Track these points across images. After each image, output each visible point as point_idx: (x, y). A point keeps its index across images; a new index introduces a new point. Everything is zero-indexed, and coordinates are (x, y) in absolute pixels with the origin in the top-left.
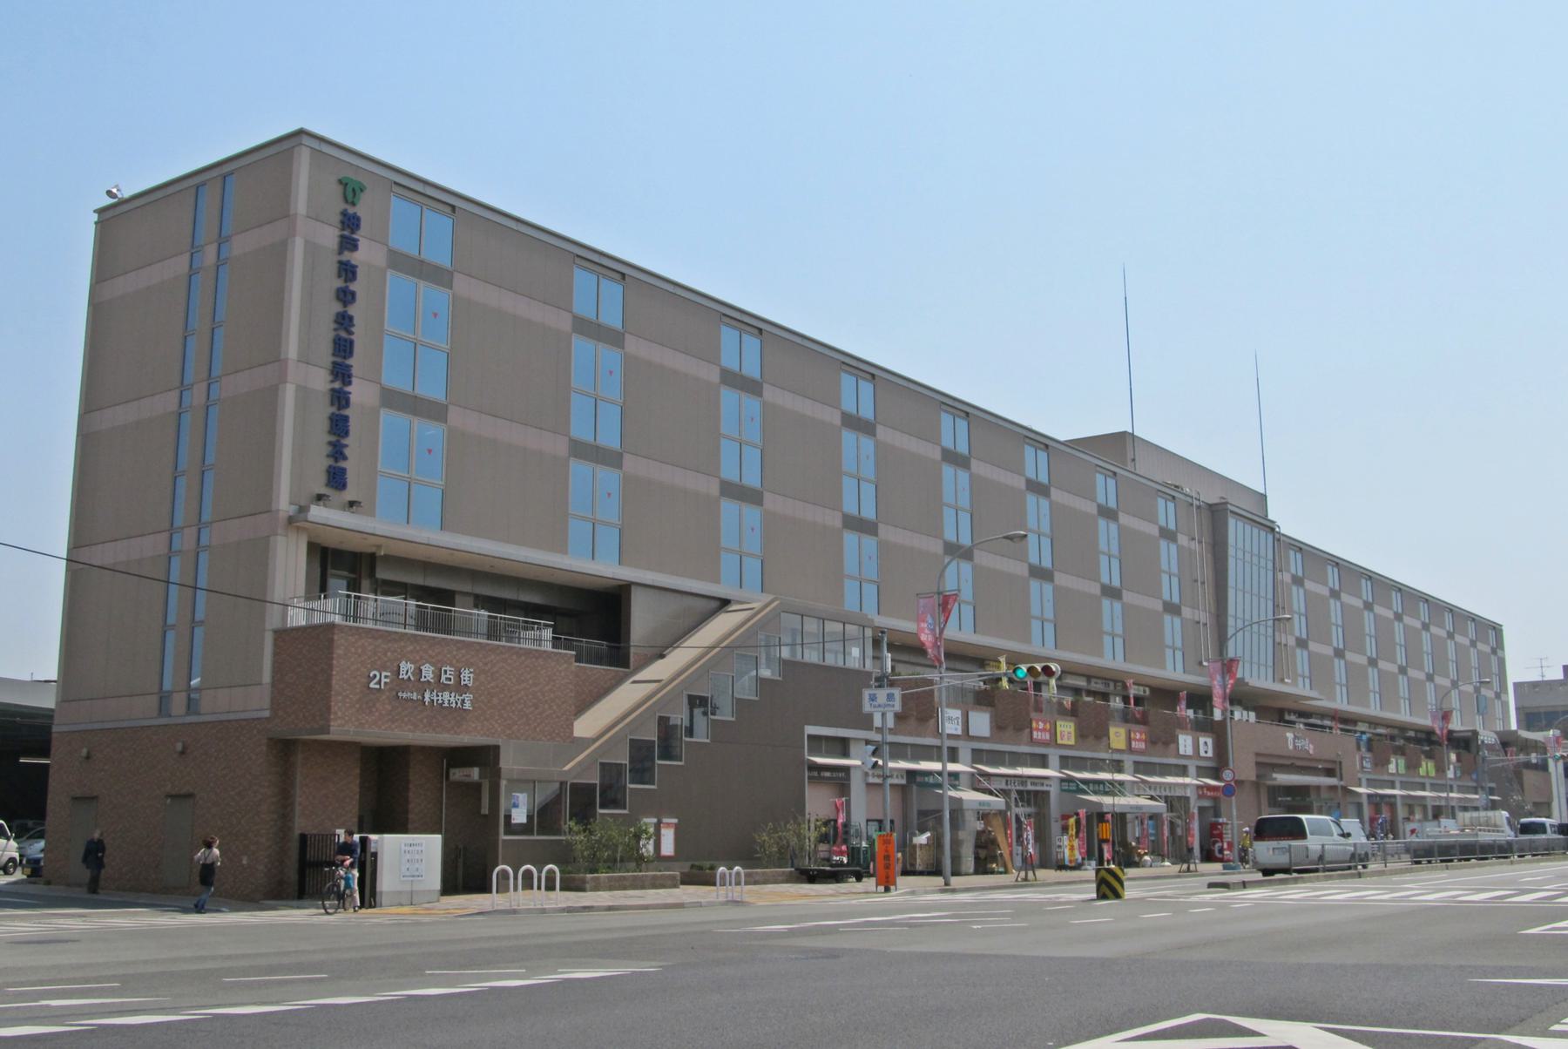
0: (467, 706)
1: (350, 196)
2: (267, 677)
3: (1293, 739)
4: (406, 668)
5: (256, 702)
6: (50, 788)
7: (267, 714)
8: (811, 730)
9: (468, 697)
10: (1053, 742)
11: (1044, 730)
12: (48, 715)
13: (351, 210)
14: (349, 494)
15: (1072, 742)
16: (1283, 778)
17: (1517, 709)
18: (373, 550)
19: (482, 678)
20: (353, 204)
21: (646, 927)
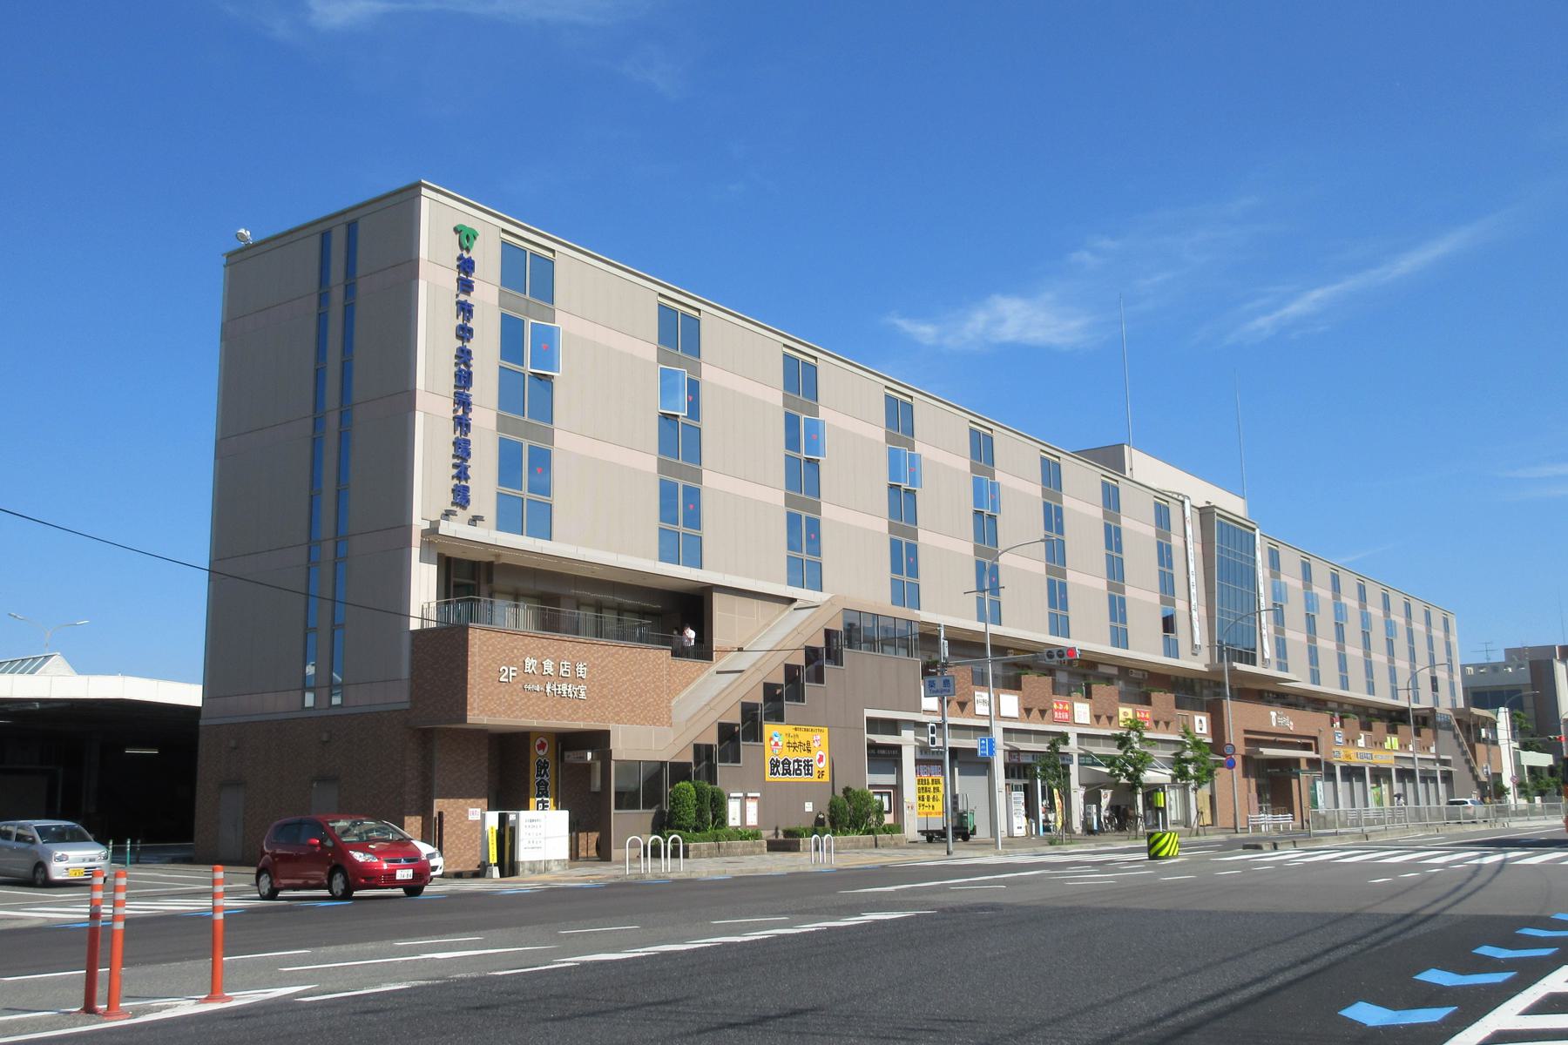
0: (583, 695)
1: (465, 243)
2: (405, 672)
3: (1277, 719)
4: (530, 663)
5: (397, 696)
6: (199, 776)
7: (407, 706)
8: (869, 713)
9: (583, 687)
10: (1071, 721)
11: (1064, 711)
12: (197, 709)
13: (466, 255)
14: (473, 510)
15: (1016, 714)
16: (1268, 752)
17: (1465, 689)
18: (492, 559)
19: (594, 671)
20: (468, 250)
21: (1193, 1005)
